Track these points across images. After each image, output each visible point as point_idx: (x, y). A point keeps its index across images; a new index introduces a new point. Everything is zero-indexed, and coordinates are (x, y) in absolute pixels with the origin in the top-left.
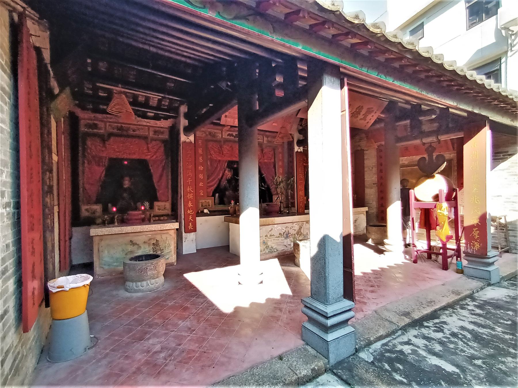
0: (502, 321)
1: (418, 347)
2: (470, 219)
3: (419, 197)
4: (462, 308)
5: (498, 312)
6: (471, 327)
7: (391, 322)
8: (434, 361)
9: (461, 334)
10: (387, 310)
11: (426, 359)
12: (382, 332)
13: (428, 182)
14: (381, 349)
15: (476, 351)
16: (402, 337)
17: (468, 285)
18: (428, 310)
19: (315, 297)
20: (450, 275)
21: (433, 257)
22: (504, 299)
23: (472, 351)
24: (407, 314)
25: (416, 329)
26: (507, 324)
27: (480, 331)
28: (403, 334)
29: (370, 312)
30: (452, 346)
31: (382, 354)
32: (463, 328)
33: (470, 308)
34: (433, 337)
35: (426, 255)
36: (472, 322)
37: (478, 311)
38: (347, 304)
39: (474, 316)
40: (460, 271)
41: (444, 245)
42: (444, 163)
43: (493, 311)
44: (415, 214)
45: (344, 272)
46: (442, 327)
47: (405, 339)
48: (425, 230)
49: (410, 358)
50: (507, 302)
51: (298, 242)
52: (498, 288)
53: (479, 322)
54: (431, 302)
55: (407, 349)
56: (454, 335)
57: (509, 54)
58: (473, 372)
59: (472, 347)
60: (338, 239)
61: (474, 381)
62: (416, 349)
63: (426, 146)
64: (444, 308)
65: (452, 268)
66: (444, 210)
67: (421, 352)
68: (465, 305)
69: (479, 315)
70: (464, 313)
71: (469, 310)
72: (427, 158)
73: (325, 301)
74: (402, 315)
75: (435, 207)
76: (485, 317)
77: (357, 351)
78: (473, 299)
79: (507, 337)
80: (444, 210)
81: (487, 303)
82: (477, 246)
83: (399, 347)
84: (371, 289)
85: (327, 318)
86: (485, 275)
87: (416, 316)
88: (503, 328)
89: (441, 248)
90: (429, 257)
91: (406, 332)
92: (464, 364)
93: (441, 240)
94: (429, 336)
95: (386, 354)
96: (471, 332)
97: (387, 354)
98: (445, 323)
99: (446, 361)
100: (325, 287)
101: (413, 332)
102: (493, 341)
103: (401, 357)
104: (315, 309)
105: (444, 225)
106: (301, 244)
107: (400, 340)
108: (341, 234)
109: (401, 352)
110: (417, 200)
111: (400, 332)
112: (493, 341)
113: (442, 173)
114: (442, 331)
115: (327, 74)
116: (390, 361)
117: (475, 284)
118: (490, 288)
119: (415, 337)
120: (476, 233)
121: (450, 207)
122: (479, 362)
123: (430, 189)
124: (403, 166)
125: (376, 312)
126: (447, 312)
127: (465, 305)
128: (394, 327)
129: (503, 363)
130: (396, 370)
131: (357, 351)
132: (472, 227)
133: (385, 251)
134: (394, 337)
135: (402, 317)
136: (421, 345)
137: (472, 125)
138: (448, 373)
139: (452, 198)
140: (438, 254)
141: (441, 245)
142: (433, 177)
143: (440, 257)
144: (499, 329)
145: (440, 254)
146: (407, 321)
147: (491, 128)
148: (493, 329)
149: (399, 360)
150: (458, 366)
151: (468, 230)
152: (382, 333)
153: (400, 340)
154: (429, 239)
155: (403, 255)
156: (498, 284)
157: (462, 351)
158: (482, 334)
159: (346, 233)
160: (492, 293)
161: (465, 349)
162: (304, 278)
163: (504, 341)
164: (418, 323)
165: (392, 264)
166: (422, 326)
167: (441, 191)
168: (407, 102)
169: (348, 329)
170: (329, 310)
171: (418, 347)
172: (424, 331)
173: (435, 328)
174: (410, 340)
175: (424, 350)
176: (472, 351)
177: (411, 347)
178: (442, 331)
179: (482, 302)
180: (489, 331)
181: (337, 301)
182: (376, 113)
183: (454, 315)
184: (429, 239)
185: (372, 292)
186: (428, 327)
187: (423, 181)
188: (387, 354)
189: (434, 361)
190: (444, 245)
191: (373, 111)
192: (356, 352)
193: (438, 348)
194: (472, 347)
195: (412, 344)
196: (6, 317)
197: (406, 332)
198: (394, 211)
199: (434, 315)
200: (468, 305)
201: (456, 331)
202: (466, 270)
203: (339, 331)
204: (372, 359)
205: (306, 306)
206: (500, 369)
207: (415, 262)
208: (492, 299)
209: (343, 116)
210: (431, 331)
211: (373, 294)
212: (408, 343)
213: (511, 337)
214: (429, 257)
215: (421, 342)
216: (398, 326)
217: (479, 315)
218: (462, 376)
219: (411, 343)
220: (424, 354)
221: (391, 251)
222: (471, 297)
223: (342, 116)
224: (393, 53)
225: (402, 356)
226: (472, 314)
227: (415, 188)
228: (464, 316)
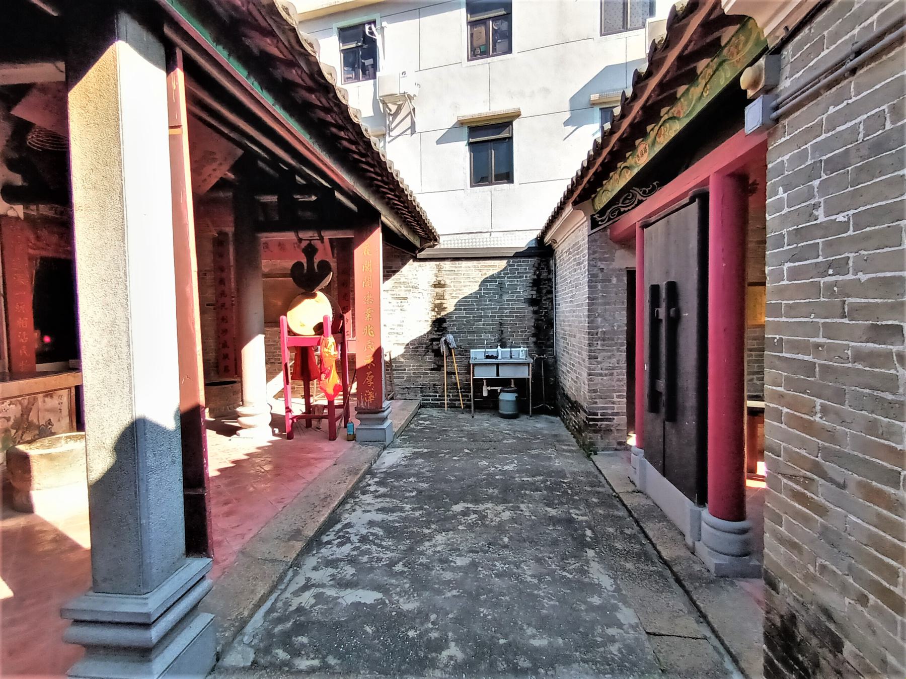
0: (408, 494)
1: (323, 586)
2: (363, 360)
3: (295, 329)
4: (364, 493)
5: (401, 483)
6: (379, 517)
7: (273, 561)
8: (350, 597)
9: (372, 534)
10: (263, 540)
11: (339, 600)
12: (261, 590)
13: (307, 303)
14: (266, 624)
15: (392, 551)
16: (297, 579)
17: (361, 455)
18: (325, 514)
19: (103, 586)
20: (341, 447)
21: (314, 423)
22: (402, 462)
23: (389, 554)
24: (296, 534)
25: (313, 555)
26: (413, 497)
27: (391, 519)
28: (296, 574)
29: (232, 559)
30: (365, 559)
31: (269, 634)
32: (371, 523)
33: (372, 488)
34: (339, 556)
35: (304, 421)
36: (378, 510)
37: (382, 490)
38: (197, 564)
39: (379, 500)
40: (352, 438)
41: (331, 402)
42: (329, 273)
43: (396, 484)
44: (289, 358)
45: (187, 498)
46: (347, 532)
47: (300, 581)
48: (302, 383)
49: (315, 615)
50: (406, 466)
51: (22, 448)
52: (393, 450)
53: (386, 505)
54: (326, 498)
55: (307, 599)
56: (364, 539)
57: (388, 139)
58: (397, 586)
59: (387, 548)
60: (170, 422)
61: (401, 600)
62: (321, 590)
63: (304, 244)
64: (343, 502)
65: (342, 433)
66: (330, 349)
67: (331, 592)
68: (365, 487)
69: (384, 495)
70: (368, 498)
71: (372, 492)
72: (305, 265)
73: (141, 585)
74: (289, 540)
75: (319, 344)
76: (390, 496)
77: (218, 657)
78: (373, 475)
79: (417, 514)
80: (330, 349)
81: (387, 474)
82: (372, 396)
83: (295, 603)
84: (226, 508)
85: (147, 626)
86: (378, 436)
87: (310, 532)
88: (411, 503)
89: (325, 407)
90: (309, 425)
91: (300, 568)
92: (385, 579)
93: (327, 395)
94: (334, 557)
95: (276, 630)
96: (382, 524)
97: (278, 629)
98: (349, 525)
99: (363, 588)
100: (140, 553)
101: (311, 561)
102: (406, 527)
103: (302, 623)
104: (109, 619)
105: (330, 371)
106: (33, 451)
107: (293, 587)
108: (179, 409)
109: (300, 610)
110: (290, 332)
111: (290, 573)
112: (406, 527)
113: (327, 291)
114: (348, 540)
115: (129, 12)
116: (286, 641)
117: (371, 451)
118: (386, 452)
119: (315, 569)
120: (369, 380)
121: (337, 343)
122: (399, 567)
123: (309, 314)
124: (266, 276)
125: (243, 553)
126: (348, 506)
127: (365, 487)
128: (281, 568)
129: (422, 553)
130: (296, 652)
131: (218, 657)
132: (365, 368)
133: (240, 428)
134: (283, 587)
135: (291, 543)
136: (327, 580)
137: (365, 219)
138: (372, 606)
139: (339, 331)
140: (320, 418)
141: (325, 403)
142: (313, 296)
143: (325, 422)
144: (408, 507)
145: (325, 417)
146: (299, 545)
147: (383, 231)
148: (402, 510)
149: (300, 628)
150: (378, 588)
151: (359, 374)
152: (262, 592)
153: (293, 587)
154: (307, 396)
155: (270, 429)
156: (392, 445)
157: (379, 560)
158: (394, 521)
159: (188, 405)
160: (392, 458)
161: (381, 555)
162: (50, 537)
163: (415, 521)
164: (314, 543)
165: (253, 450)
166: (321, 544)
167: (325, 318)
168: (275, 160)
169: (202, 620)
170: (152, 603)
171: (323, 586)
172: (325, 552)
173: (339, 540)
174: (308, 579)
175: (332, 586)
176: (389, 554)
177: (313, 591)
178: (348, 540)
179: (382, 476)
180: (399, 514)
181: (172, 569)
182: (221, 164)
183: (357, 507)
184: (307, 396)
185: (228, 514)
186: (329, 543)
187: (299, 302)
188: (278, 629)
189: (350, 597)
190: (331, 402)
191: (214, 160)
192: (218, 660)
193: (349, 571)
194: (387, 548)
195: (313, 585)
196: (898, 50)
197: (300, 568)
198: (254, 353)
199: (333, 520)
200: (370, 485)
201: (364, 531)
202: (359, 435)
203: (178, 639)
204: (252, 656)
205: (77, 622)
206: (421, 564)
207: (290, 437)
208: (391, 467)
209: (174, 140)
210: (335, 548)
211: (232, 518)
212: (306, 587)
213: (421, 512)
214: (309, 425)
215: (323, 575)
216: (287, 563)
217: (384, 495)
218: (387, 602)
219: (317, 587)
220: (331, 592)
221: (250, 427)
222: (370, 472)
223: (172, 137)
224: (280, 45)
225: (302, 618)
226: (377, 497)
227: (289, 313)
228: (369, 504)
